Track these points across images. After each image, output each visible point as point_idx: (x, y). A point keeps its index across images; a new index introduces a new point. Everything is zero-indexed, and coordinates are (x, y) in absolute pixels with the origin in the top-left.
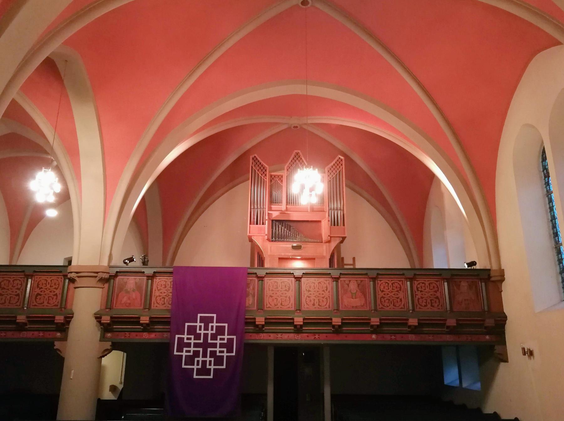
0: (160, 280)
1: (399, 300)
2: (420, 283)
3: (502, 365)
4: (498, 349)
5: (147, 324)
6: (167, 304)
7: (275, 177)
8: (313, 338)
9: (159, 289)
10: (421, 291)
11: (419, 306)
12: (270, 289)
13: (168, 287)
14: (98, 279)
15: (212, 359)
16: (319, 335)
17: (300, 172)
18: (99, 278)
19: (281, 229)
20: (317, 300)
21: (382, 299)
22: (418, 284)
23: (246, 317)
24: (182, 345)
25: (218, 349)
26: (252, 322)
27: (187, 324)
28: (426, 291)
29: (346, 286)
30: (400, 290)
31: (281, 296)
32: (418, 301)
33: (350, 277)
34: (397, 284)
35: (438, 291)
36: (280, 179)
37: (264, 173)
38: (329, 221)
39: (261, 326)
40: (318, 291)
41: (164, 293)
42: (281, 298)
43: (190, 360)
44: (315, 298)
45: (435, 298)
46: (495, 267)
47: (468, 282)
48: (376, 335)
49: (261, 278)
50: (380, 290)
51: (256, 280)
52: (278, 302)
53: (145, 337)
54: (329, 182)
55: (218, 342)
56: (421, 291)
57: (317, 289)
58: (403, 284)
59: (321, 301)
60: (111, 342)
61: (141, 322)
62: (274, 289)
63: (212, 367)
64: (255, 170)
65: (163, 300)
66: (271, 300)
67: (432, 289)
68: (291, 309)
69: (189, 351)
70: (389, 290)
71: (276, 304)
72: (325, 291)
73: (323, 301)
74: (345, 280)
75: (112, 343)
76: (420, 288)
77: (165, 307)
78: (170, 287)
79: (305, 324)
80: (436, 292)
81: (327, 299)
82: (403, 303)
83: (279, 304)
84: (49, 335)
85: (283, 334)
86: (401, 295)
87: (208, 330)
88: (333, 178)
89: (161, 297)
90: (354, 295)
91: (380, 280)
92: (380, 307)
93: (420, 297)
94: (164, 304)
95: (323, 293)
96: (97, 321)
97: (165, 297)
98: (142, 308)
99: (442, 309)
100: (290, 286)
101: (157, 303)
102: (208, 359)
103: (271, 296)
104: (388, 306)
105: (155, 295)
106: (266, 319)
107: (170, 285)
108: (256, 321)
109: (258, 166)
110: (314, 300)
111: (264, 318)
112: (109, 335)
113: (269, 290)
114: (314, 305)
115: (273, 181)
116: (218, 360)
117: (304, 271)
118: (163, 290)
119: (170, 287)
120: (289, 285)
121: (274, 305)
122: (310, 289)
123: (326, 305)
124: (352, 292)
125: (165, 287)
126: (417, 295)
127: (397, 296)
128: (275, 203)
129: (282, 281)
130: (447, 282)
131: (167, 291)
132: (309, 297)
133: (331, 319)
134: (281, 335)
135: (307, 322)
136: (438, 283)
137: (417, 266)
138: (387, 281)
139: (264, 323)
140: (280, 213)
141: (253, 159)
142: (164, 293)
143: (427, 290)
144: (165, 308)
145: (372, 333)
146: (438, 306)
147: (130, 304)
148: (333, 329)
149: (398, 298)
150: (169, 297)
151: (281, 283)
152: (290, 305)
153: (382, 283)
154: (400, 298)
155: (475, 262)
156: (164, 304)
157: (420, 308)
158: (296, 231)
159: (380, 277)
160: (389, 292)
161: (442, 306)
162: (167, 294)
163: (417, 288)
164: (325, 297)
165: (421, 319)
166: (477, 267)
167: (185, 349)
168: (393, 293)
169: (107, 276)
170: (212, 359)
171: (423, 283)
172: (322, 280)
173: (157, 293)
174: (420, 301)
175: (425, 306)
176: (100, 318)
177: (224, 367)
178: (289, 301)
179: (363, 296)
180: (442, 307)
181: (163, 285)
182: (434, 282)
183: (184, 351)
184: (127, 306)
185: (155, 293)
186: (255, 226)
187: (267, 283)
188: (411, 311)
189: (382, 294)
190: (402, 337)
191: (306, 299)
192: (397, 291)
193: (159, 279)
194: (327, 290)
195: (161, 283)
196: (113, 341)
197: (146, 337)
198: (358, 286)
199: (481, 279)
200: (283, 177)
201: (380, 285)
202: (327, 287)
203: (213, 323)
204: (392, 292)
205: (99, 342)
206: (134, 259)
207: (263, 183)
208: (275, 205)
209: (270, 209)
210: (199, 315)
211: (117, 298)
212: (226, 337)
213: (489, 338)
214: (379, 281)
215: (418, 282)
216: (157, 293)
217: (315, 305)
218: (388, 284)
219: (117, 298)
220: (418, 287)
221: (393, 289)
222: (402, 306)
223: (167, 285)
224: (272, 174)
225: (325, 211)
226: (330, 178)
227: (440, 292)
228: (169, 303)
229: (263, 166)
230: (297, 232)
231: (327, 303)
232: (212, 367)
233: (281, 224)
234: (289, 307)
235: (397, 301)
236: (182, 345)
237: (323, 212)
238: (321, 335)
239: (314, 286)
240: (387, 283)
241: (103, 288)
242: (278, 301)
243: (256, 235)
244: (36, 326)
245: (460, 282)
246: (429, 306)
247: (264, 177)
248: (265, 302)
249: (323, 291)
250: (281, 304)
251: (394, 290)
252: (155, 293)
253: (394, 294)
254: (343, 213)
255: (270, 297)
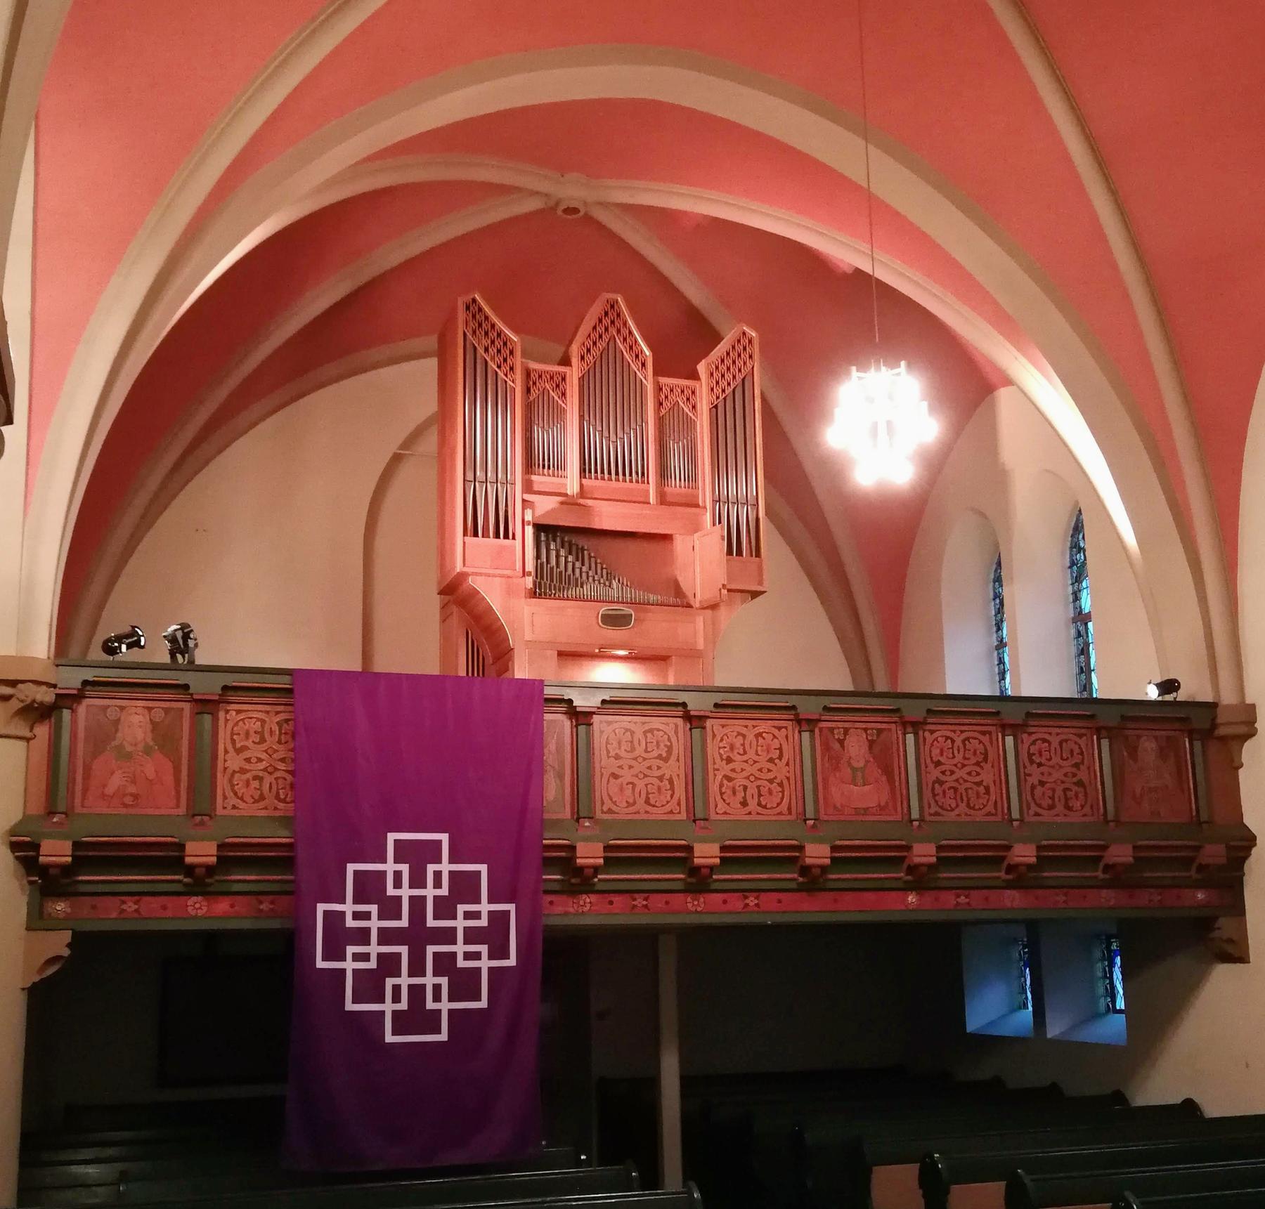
0: (242, 716)
1: (982, 789)
2: (1037, 740)
3: (1222, 973)
4: (1225, 926)
5: (210, 870)
6: (270, 800)
7: (540, 376)
8: (740, 905)
9: (238, 745)
10: (1040, 765)
11: (1034, 808)
12: (612, 753)
13: (271, 741)
14: (15, 705)
15: (444, 981)
16: (757, 898)
17: (860, 378)
18: (22, 701)
19: (558, 556)
20: (752, 790)
21: (936, 785)
22: (1031, 744)
23: (545, 842)
24: (339, 936)
25: (460, 948)
26: (565, 860)
27: (351, 868)
28: (1051, 763)
29: (837, 746)
30: (986, 760)
31: (646, 776)
32: (1033, 795)
33: (880, 719)
34: (977, 741)
35: (1082, 762)
36: (558, 386)
37: (505, 360)
38: (723, 538)
39: (203, 870)
40: (755, 762)
41: (260, 760)
42: (647, 780)
43: (370, 985)
44: (746, 782)
45: (1074, 783)
46: (1228, 697)
47: (1156, 738)
48: (918, 894)
49: (580, 717)
50: (932, 760)
51: (567, 723)
52: (637, 795)
53: (193, 913)
54: (714, 409)
55: (460, 924)
56: (1040, 765)
57: (640, 751)
58: (991, 743)
59: (764, 791)
60: (71, 931)
61: (41, 859)
62: (623, 754)
63: (445, 1006)
64: (475, 349)
65: (255, 784)
66: (614, 790)
67: (1068, 758)
68: (678, 817)
69: (365, 957)
70: (955, 761)
71: (631, 801)
72: (777, 761)
73: (770, 792)
74: (833, 728)
75: (75, 935)
76: (1037, 755)
77: (266, 808)
78: (279, 742)
79: (942, 862)
80: (1076, 765)
81: (781, 785)
82: (993, 798)
83: (641, 801)
84: (164, 908)
85: (972, 892)
86: (987, 776)
87: (423, 885)
88: (725, 399)
89: (248, 775)
90: (859, 774)
91: (930, 731)
92: (932, 811)
93: (1036, 782)
94: (262, 798)
95: (770, 766)
96: (17, 858)
97: (261, 774)
98: (182, 810)
99: (1093, 815)
100: (671, 744)
101: (236, 794)
102: (429, 980)
103: (615, 776)
104: (952, 810)
105: (225, 769)
106: (607, 848)
107: (277, 733)
108: (578, 855)
109: (486, 334)
110: (745, 788)
111: (601, 846)
112: (61, 907)
113: (609, 757)
114: (744, 803)
115: (534, 393)
116: (464, 984)
117: (719, 698)
118: (256, 752)
119: (279, 742)
120: (669, 740)
121: (625, 805)
122: (941, 759)
123: (778, 805)
124: (855, 765)
125: (263, 740)
126: (1030, 775)
127: (978, 779)
128: (549, 468)
129: (647, 727)
130: (1109, 738)
131: (270, 756)
132: (730, 779)
133: (801, 848)
134: (646, 899)
135: (733, 858)
136: (1082, 742)
137: (881, 687)
138: (948, 734)
139: (828, 861)
140: (562, 503)
141: (468, 308)
142: (260, 760)
143: (1056, 760)
144: (263, 813)
145: (908, 888)
146: (1082, 806)
147: (136, 797)
148: (801, 879)
149: (979, 784)
150: (278, 774)
151: (645, 733)
152: (672, 805)
153: (936, 739)
154: (984, 784)
155: (1176, 681)
156: (262, 798)
157: (1037, 814)
158: (599, 566)
159: (1032, 723)
160: (956, 765)
161: (1092, 807)
162: (271, 765)
163: (1030, 755)
164: (778, 781)
165: (1045, 846)
166: (1181, 696)
167: (351, 950)
168: (967, 769)
169: (46, 696)
170: (444, 981)
171: (1044, 741)
172: (656, 723)
173: (234, 762)
174: (1039, 791)
175: (1051, 807)
176: (36, 847)
177: (483, 1004)
178: (670, 792)
179: (884, 778)
180: (1093, 811)
181: (252, 733)
182: (976, 735)
183: (349, 956)
184: (126, 806)
185: (225, 761)
186: (491, 540)
187: (602, 732)
188: (811, 822)
189: (935, 773)
190: (780, 901)
191: (721, 786)
192: (978, 764)
193: (238, 712)
194: (780, 758)
195: (247, 727)
196: (78, 929)
197: (200, 913)
198: (870, 747)
199: (1098, 730)
200: (568, 380)
201: (932, 745)
202: (780, 749)
203: (440, 862)
204: (964, 766)
205: (26, 932)
206: (142, 639)
207: (502, 398)
208: (544, 475)
209: (528, 487)
210: (392, 837)
211: (87, 777)
212: (485, 907)
213: (1203, 896)
214: (927, 734)
215: (1034, 737)
216: (234, 762)
217: (747, 805)
218: (953, 741)
219: (87, 777)
220: (1031, 752)
221: (965, 758)
222: (990, 808)
223: (267, 735)
224: (533, 365)
225: (701, 504)
226: (718, 398)
227: (1089, 768)
228: (277, 797)
229: (502, 336)
230: (602, 569)
231: (782, 799)
232: (445, 1006)
233: (558, 540)
234: (671, 812)
235: (978, 793)
236: (339, 936)
237: (693, 510)
238: (653, 897)
239: (743, 745)
240: (951, 739)
241: (28, 740)
242: (637, 790)
243: (483, 571)
244: (985, 875)
245: (1139, 737)
246: (1060, 808)
247: (506, 375)
248: (597, 794)
249: (771, 760)
250: (647, 802)
251: (968, 759)
252: (225, 761)
253: (969, 774)
254: (755, 516)
255: (611, 779)
